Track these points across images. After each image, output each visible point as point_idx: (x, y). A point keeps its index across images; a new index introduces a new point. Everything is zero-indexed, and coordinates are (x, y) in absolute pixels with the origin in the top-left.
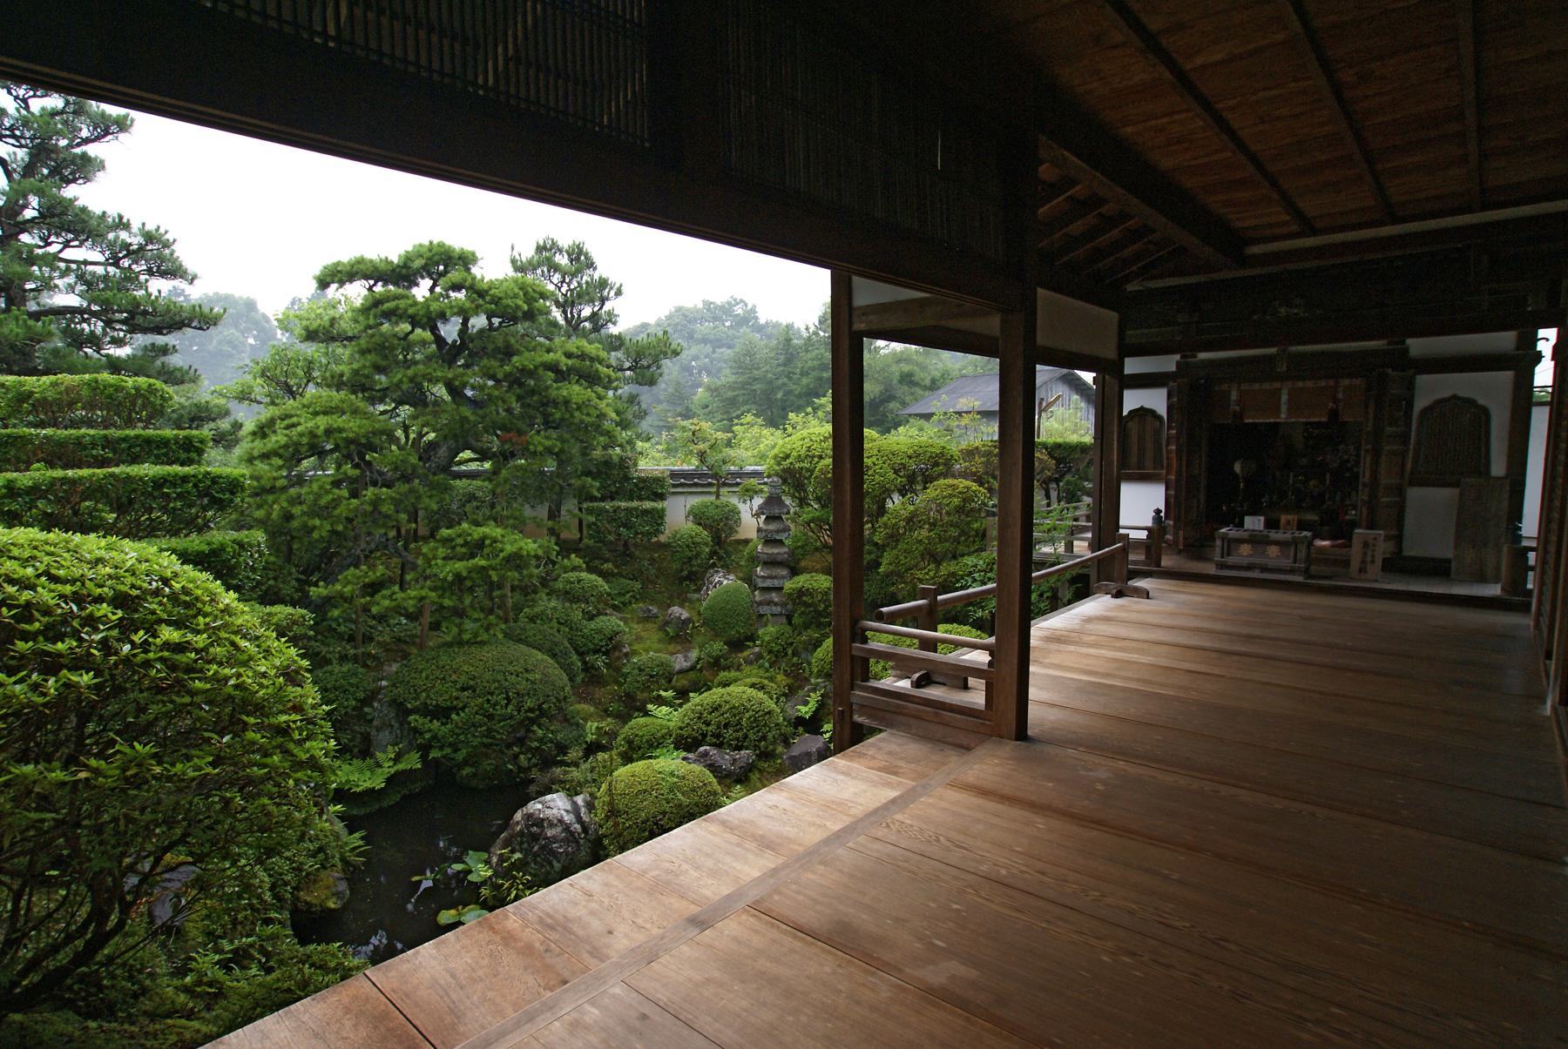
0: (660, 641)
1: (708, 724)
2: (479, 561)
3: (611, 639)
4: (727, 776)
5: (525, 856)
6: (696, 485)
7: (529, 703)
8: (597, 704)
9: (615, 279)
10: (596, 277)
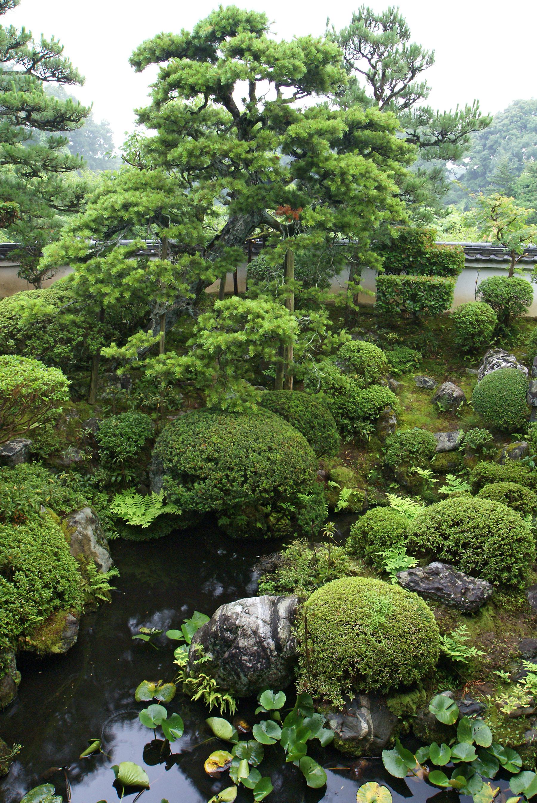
0: (429, 415)
1: (446, 538)
2: (241, 336)
3: (380, 409)
4: (455, 606)
5: (216, 658)
6: (491, 261)
7: (265, 484)
8: (357, 468)
9: (426, 48)
10: (408, 45)
